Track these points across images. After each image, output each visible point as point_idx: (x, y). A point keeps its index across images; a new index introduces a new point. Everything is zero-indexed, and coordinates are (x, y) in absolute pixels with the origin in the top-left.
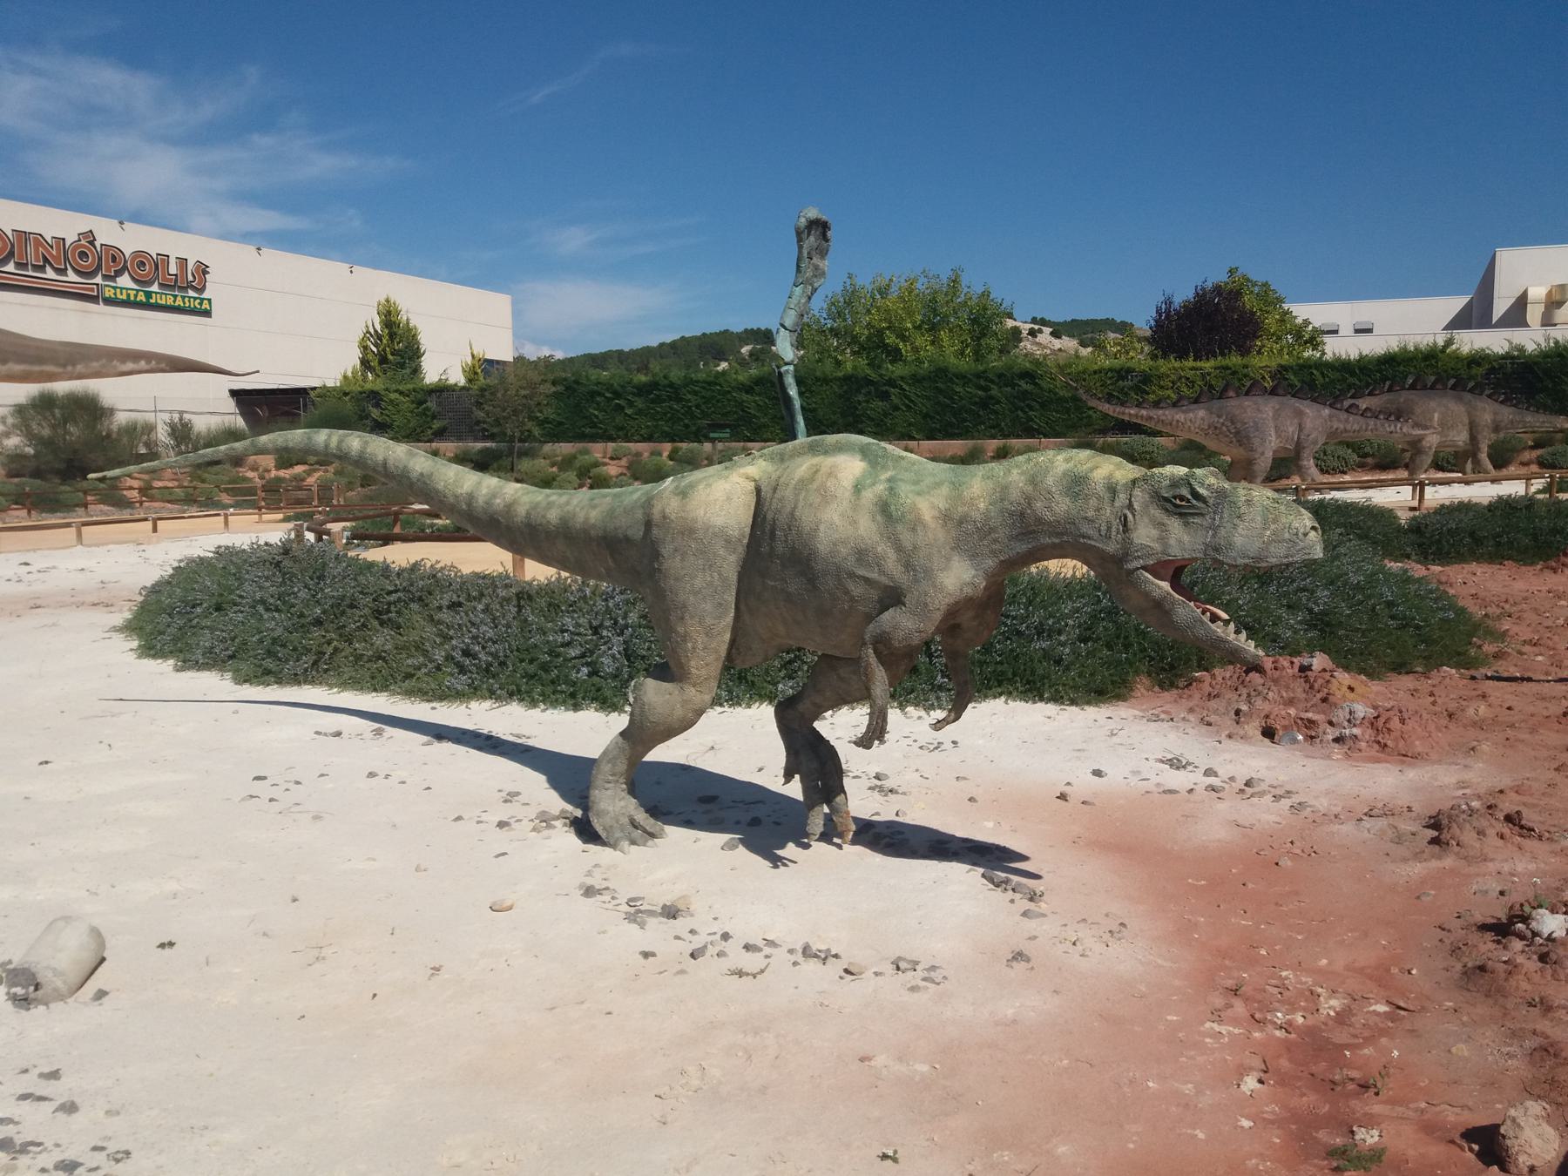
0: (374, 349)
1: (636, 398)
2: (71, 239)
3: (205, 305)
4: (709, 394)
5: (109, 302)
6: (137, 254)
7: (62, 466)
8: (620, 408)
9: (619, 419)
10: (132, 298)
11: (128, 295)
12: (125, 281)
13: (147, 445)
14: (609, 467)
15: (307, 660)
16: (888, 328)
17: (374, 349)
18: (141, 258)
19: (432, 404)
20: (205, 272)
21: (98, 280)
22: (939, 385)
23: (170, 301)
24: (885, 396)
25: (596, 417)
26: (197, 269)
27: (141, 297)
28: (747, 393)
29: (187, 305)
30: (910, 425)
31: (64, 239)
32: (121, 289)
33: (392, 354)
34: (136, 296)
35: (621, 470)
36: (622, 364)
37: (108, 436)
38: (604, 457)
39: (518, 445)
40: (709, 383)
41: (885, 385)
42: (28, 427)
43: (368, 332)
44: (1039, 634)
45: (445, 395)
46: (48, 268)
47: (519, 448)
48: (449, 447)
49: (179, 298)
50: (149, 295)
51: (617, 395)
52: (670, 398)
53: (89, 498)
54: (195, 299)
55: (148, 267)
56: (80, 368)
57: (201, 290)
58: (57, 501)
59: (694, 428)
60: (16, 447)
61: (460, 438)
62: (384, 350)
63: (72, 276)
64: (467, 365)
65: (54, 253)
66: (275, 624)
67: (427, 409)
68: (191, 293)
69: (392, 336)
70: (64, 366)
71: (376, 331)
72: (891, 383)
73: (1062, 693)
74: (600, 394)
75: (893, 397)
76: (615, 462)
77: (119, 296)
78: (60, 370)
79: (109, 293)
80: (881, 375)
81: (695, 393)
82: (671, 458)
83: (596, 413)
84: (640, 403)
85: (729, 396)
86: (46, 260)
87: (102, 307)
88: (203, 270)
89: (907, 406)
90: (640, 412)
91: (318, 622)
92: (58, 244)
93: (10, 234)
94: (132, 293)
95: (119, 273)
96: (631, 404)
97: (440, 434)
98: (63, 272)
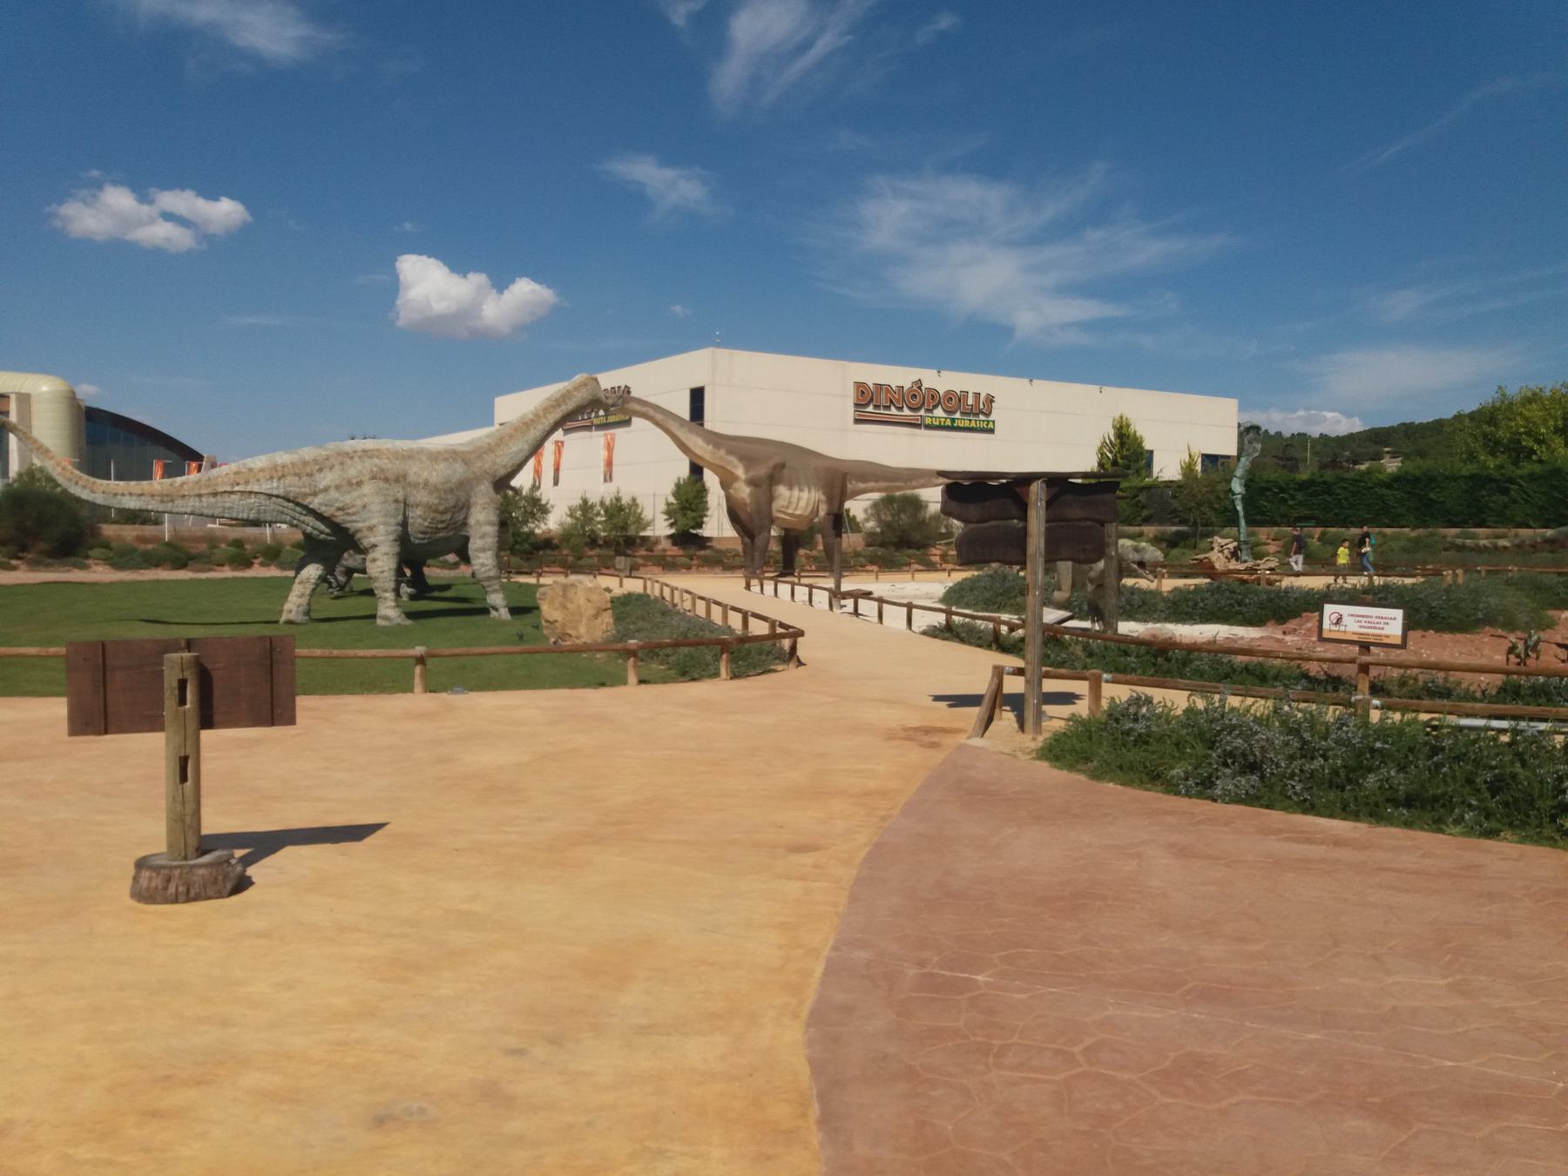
0: (1110, 455)
1: (1297, 493)
2: (907, 386)
3: (991, 425)
4: (1355, 490)
5: (928, 427)
6: (948, 392)
7: (896, 540)
8: (1284, 500)
9: (1283, 509)
10: (942, 424)
11: (940, 422)
12: (939, 412)
13: (946, 527)
14: (1270, 546)
15: (996, 606)
16: (1525, 433)
17: (1110, 455)
18: (950, 395)
19: (1142, 498)
20: (992, 401)
21: (922, 412)
22: (1554, 482)
23: (967, 424)
24: (1505, 491)
25: (1265, 507)
26: (987, 398)
27: (949, 423)
28: (1387, 488)
30: (1527, 515)
31: (903, 387)
32: (936, 418)
33: (1122, 458)
34: (945, 422)
35: (1278, 549)
36: (1409, 438)
37: (924, 521)
38: (1268, 539)
39: (1200, 528)
40: (1356, 481)
41: (1506, 482)
42: (879, 515)
43: (1105, 442)
45: (1153, 490)
46: (892, 407)
47: (1201, 531)
48: (1150, 530)
49: (973, 422)
50: (953, 420)
51: (1283, 490)
52: (1324, 493)
53: (912, 561)
54: (984, 421)
55: (954, 401)
56: (914, 483)
57: (988, 415)
58: (893, 562)
59: (1342, 517)
60: (872, 528)
61: (1162, 523)
62: (1115, 456)
63: (906, 412)
64: (1185, 463)
65: (897, 397)
66: (987, 594)
67: (1139, 501)
68: (982, 417)
69: (1122, 444)
70: (906, 483)
71: (1111, 442)
72: (1511, 481)
74: (1268, 489)
75: (1513, 493)
76: (1276, 542)
77: (934, 423)
78: (903, 484)
79: (928, 421)
80: (1502, 475)
81: (1345, 488)
82: (1319, 539)
83: (1265, 504)
84: (1300, 496)
85: (1372, 491)
86: (891, 401)
87: (923, 431)
88: (990, 400)
89: (1526, 501)
90: (1300, 504)
91: (1002, 595)
92: (899, 390)
93: (871, 386)
94: (943, 420)
95: (935, 407)
96: (1293, 497)
97: (1147, 520)
98: (901, 409)
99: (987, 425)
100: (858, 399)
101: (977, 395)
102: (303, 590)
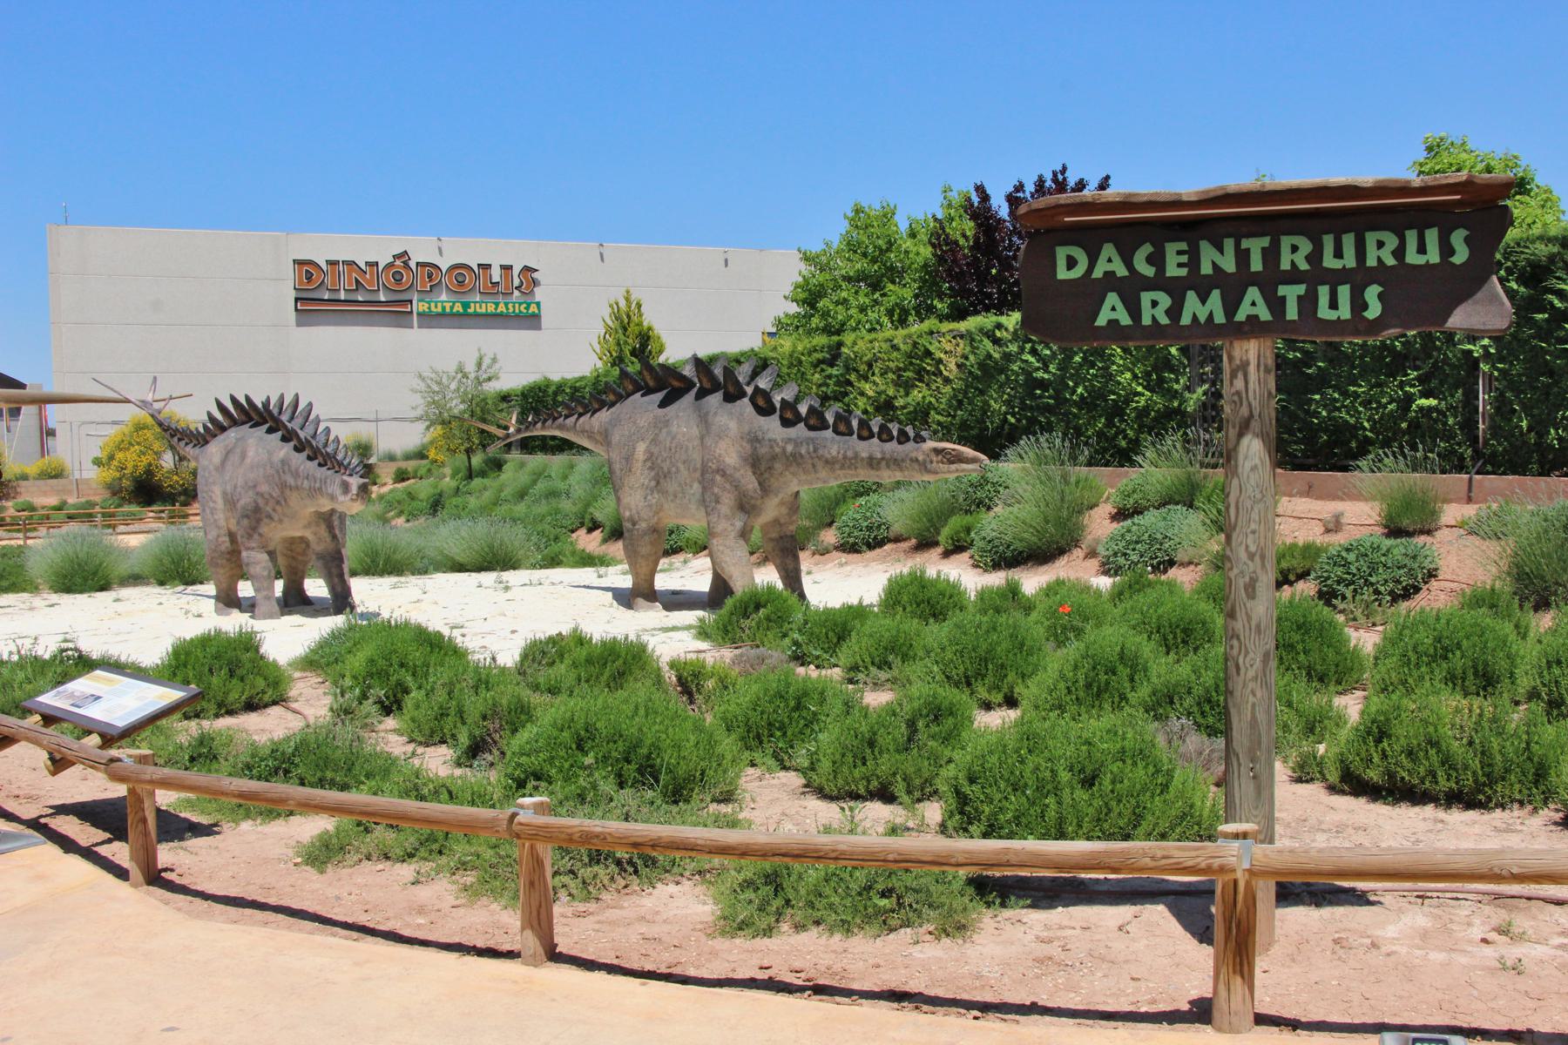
3: (533, 309)
11: (444, 308)
23: (491, 309)
27: (458, 308)
29: (511, 310)
34: (452, 308)
44: (580, 748)
49: (502, 305)
73: (1263, 606)
99: (527, 308)
100: (301, 282)
101: (507, 268)
102: (359, 610)
